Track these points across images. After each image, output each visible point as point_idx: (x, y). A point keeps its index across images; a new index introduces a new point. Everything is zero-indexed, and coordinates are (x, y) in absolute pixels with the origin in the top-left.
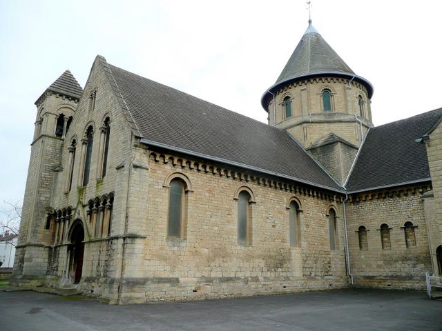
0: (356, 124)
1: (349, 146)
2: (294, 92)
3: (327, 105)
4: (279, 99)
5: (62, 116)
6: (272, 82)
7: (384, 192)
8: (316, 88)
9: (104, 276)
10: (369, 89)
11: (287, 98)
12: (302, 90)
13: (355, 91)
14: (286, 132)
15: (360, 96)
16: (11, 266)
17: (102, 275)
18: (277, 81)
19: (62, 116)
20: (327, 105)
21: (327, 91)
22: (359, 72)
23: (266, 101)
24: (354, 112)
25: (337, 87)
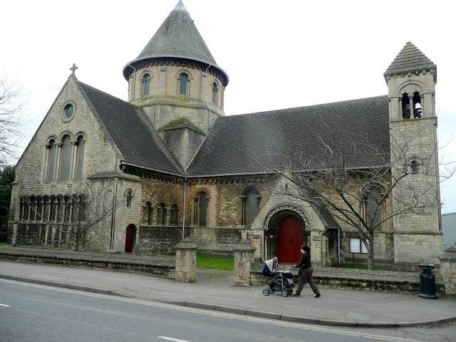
0: (205, 111)
1: (196, 132)
2: (154, 70)
3: (183, 90)
4: (138, 74)
5: (405, 95)
6: (134, 56)
7: (226, 179)
8: (174, 71)
9: (59, 225)
10: (224, 79)
11: (147, 75)
12: (162, 71)
13: (210, 78)
14: (142, 111)
15: (215, 84)
16: (436, 282)
17: (61, 227)
18: (138, 57)
19: (405, 95)
20: (183, 90)
21: (184, 75)
22: (221, 64)
23: (128, 72)
24: (207, 97)
25: (194, 73)
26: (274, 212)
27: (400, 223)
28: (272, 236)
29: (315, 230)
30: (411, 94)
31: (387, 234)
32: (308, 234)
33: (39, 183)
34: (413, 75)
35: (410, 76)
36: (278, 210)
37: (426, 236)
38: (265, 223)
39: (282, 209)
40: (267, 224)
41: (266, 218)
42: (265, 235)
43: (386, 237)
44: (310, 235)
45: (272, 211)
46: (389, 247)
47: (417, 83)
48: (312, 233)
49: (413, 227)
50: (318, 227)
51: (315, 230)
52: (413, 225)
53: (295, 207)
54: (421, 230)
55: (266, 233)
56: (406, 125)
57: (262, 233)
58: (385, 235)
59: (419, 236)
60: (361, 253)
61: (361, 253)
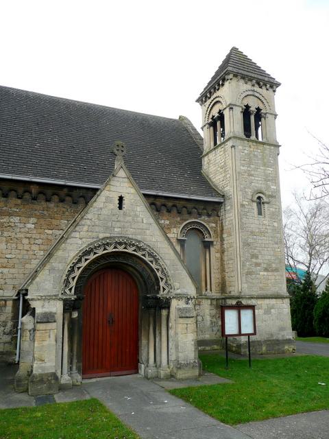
19: (247, 107)
26: (92, 257)
27: (247, 282)
28: (75, 315)
29: (179, 297)
30: (253, 109)
31: (212, 299)
32: (166, 304)
33: (211, 397)
34: (256, 85)
35: (253, 85)
36: (100, 252)
37: (273, 301)
38: (67, 282)
39: (110, 249)
40: (73, 284)
41: (72, 270)
42: (65, 310)
43: (211, 304)
44: (168, 308)
45: (87, 253)
46: (214, 320)
47: (260, 97)
48: (174, 304)
49: (261, 289)
50: (185, 291)
51: (179, 297)
52: (261, 285)
53: (139, 248)
54: (269, 293)
55: (69, 306)
56: (250, 147)
57: (57, 308)
58: (209, 301)
59: (267, 301)
60: (240, 334)
61: (240, 334)
